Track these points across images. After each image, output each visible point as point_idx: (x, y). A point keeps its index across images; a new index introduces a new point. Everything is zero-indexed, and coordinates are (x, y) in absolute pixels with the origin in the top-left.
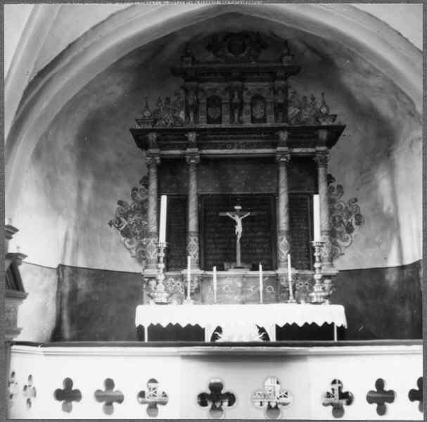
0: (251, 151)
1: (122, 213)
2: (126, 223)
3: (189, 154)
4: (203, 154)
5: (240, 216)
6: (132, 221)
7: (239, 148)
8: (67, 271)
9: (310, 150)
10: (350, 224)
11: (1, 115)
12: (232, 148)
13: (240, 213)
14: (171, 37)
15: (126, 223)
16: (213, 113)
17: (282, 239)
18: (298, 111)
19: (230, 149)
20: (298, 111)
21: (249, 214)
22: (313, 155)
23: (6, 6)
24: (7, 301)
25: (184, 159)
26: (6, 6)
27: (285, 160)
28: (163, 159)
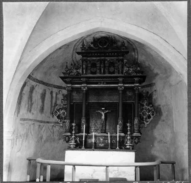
0: (108, 85)
1: (58, 109)
2: (59, 113)
3: (83, 86)
4: (88, 86)
5: (104, 112)
6: (61, 112)
7: (103, 84)
8: (82, 103)
9: (133, 85)
10: (149, 115)
11: (0, 30)
12: (101, 84)
13: (103, 111)
14: (71, 43)
15: (59, 113)
16: (93, 70)
17: (119, 122)
18: (128, 69)
19: (100, 84)
20: (128, 69)
21: (107, 111)
22: (134, 87)
23: (3, 3)
24: (66, 179)
25: (81, 88)
26: (3, 3)
27: (122, 89)
28: (72, 88)
